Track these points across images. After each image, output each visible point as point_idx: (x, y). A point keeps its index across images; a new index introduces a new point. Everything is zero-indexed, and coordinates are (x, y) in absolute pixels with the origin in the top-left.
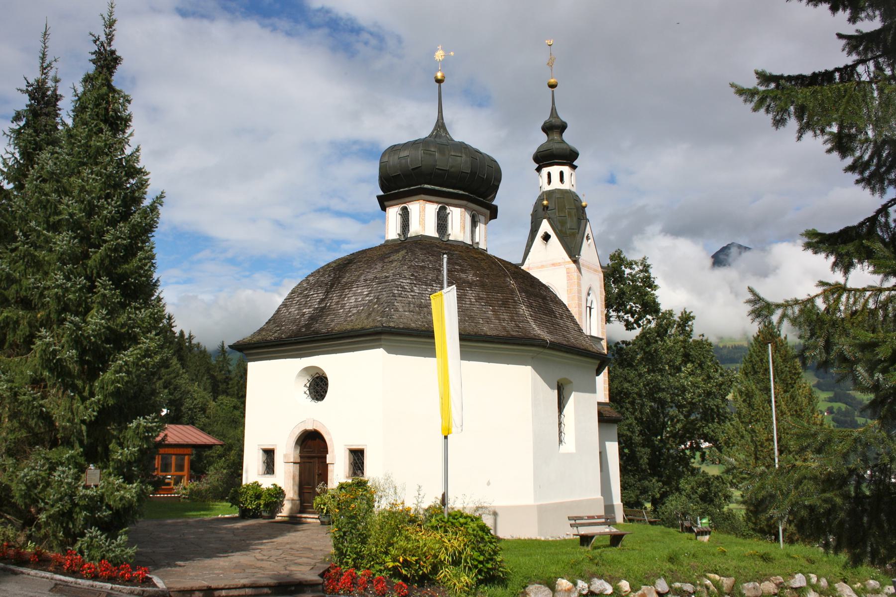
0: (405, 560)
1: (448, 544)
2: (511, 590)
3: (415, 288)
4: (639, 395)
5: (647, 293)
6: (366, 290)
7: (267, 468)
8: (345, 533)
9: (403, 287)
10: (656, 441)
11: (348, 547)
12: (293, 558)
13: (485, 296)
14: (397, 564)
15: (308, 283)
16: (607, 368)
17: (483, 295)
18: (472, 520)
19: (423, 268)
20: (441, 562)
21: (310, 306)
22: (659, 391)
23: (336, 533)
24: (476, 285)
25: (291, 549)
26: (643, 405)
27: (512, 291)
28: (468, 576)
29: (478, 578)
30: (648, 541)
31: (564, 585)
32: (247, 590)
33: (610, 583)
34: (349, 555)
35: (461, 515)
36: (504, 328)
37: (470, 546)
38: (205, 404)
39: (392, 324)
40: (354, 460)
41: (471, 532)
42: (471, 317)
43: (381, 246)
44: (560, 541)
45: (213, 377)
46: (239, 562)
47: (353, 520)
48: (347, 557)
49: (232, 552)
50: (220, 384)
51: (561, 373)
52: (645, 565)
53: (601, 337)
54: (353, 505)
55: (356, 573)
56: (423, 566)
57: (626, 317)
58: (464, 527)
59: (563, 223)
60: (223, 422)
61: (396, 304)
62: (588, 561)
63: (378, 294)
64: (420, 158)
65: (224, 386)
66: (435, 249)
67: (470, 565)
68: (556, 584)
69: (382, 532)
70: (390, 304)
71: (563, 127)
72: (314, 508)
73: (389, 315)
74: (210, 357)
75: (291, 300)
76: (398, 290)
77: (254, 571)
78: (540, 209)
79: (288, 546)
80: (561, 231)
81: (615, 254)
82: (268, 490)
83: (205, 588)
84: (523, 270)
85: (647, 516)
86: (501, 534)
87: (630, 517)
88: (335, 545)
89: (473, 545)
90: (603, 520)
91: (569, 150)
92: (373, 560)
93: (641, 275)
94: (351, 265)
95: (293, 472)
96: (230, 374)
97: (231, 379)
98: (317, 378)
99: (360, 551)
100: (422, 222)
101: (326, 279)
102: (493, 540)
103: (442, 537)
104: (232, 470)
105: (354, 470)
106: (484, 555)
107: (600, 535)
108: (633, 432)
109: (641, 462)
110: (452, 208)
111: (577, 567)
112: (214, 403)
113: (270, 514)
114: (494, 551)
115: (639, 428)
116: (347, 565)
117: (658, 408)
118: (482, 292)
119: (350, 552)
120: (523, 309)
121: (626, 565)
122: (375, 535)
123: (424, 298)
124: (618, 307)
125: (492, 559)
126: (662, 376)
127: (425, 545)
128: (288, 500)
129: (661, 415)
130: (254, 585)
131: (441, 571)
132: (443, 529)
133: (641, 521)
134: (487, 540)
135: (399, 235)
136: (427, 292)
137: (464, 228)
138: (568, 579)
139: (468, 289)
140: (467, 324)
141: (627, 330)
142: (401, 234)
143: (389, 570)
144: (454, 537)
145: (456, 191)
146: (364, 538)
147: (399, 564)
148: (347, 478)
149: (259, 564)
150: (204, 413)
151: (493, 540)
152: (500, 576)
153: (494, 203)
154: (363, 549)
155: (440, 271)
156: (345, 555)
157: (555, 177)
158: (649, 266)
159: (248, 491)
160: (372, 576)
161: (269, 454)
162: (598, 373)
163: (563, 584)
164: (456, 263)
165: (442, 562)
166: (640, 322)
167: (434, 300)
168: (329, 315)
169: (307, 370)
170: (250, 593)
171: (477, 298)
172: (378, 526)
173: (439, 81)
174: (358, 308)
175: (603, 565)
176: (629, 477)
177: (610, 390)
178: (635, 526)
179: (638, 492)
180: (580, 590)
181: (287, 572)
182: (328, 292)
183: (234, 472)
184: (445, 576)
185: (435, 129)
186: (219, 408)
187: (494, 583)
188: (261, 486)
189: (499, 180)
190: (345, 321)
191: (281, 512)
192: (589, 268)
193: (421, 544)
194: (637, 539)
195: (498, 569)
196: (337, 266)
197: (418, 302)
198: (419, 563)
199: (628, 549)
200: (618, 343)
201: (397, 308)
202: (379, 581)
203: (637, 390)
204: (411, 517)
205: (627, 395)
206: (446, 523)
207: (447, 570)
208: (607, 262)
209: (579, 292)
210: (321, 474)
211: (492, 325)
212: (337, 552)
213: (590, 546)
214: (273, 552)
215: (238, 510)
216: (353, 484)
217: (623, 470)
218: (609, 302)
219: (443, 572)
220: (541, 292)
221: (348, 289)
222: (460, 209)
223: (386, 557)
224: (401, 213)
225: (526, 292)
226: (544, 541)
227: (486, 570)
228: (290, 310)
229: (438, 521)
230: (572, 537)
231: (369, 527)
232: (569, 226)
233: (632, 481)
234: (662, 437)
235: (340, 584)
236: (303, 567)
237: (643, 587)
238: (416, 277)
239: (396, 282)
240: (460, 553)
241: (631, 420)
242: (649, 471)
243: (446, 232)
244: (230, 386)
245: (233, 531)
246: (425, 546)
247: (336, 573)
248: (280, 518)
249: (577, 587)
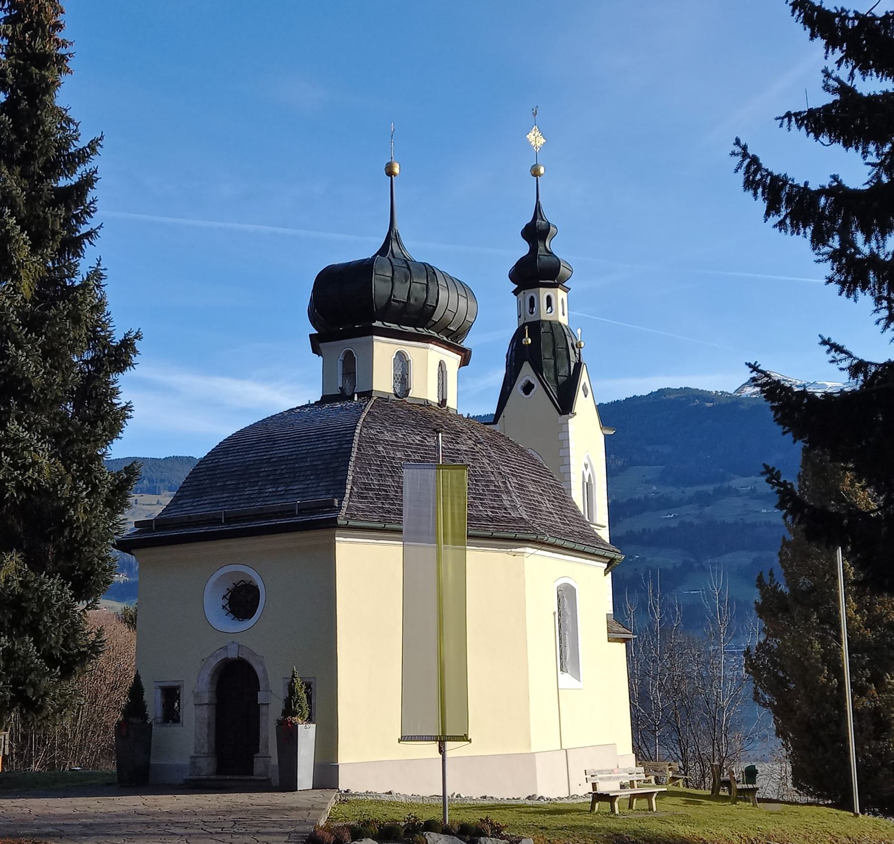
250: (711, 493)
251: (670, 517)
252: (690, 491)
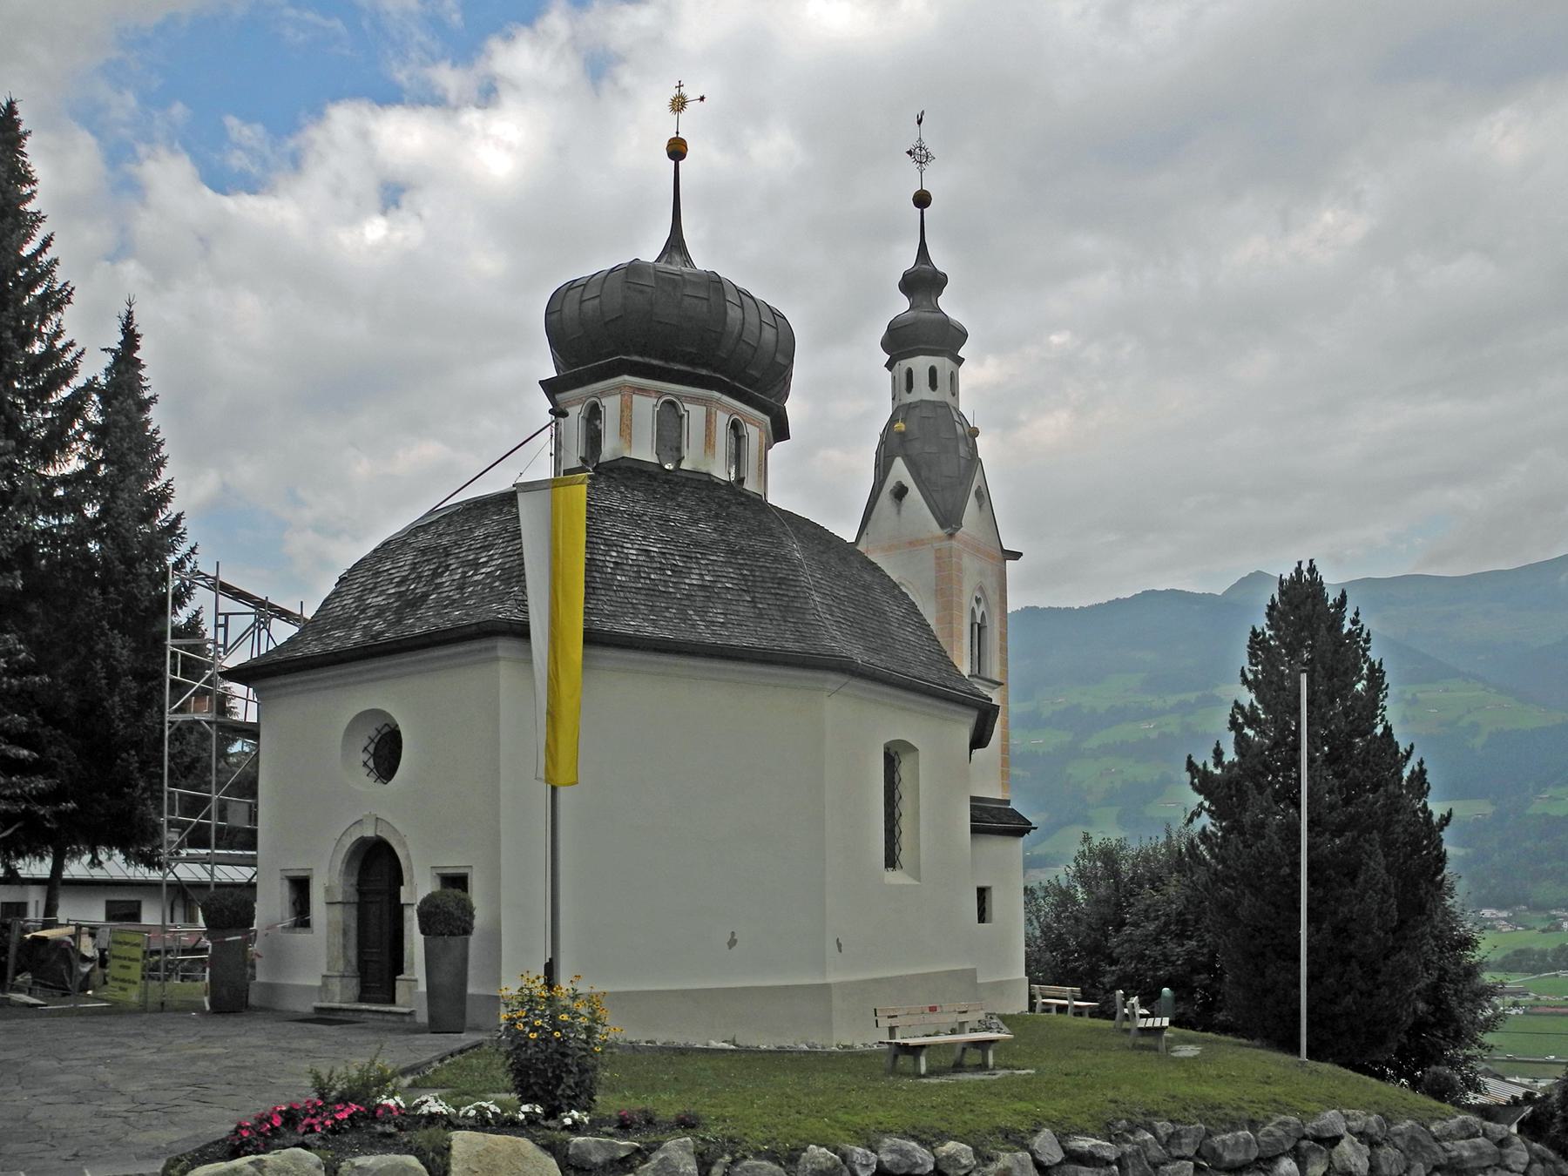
157: (921, 379)
161: (300, 886)
250: (1193, 701)
251: (1148, 728)
252: (1172, 700)
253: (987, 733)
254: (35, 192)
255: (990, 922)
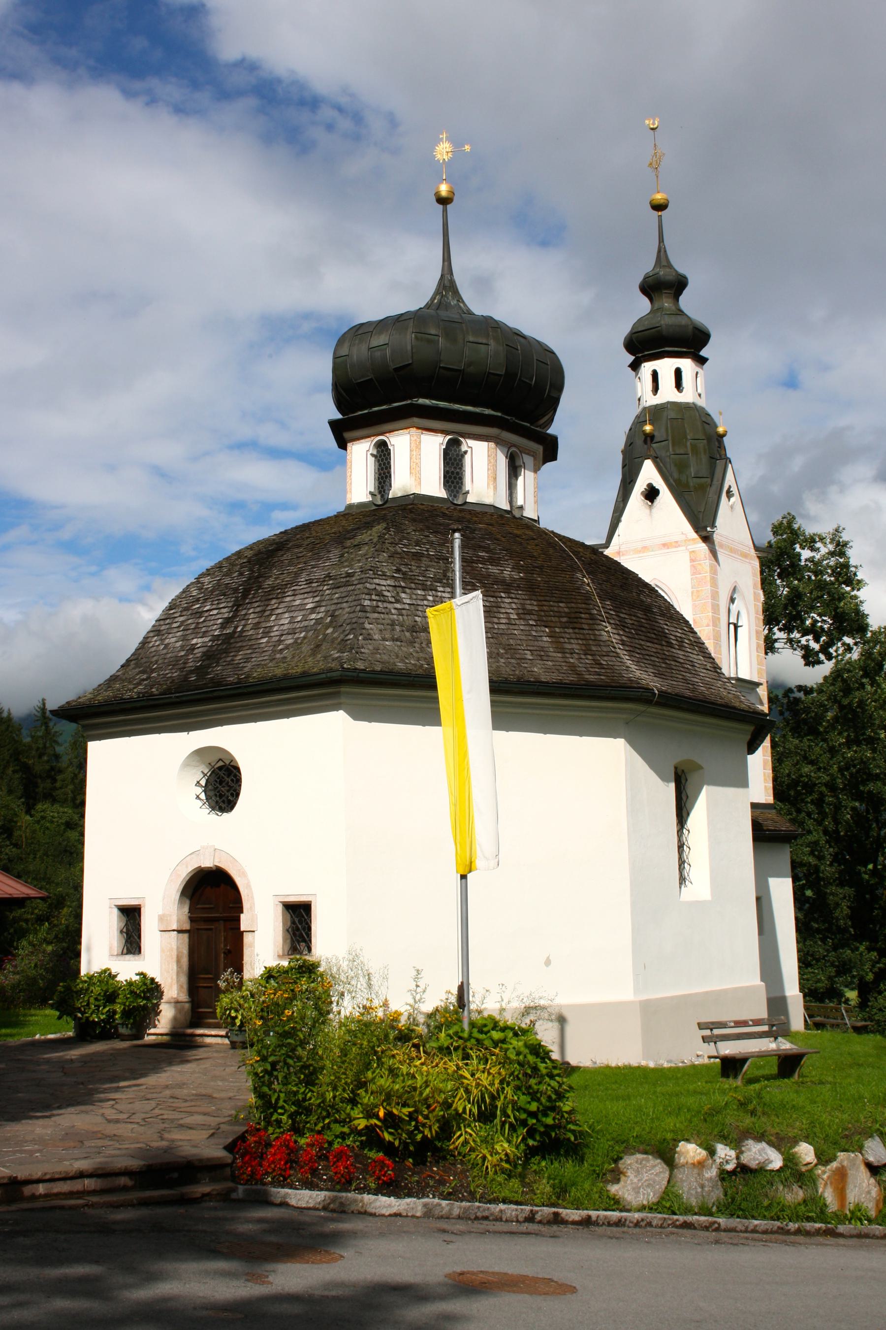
0: (389, 1114)
1: (470, 1081)
2: (592, 1165)
3: (403, 595)
4: (831, 787)
5: (842, 596)
6: (311, 600)
7: (126, 941)
8: (274, 1065)
9: (380, 594)
10: (865, 873)
11: (280, 1091)
12: (177, 1115)
13: (536, 608)
14: (374, 1121)
15: (200, 589)
16: (768, 738)
17: (532, 605)
18: (516, 1034)
19: (417, 556)
20: (458, 1116)
21: (205, 632)
22: (868, 780)
23: (256, 1065)
24: (519, 588)
25: (172, 1097)
26: (838, 807)
27: (587, 598)
28: (509, 1142)
29: (527, 1145)
30: (851, 1066)
31: (692, 1154)
32: (87, 1181)
33: (778, 1148)
34: (282, 1107)
35: (495, 1025)
36: (573, 667)
37: (512, 1084)
38: (11, 821)
39: (360, 665)
40: (293, 922)
41: (513, 1057)
42: (509, 648)
43: (339, 516)
44: (684, 1068)
45: (26, 769)
46: (73, 1126)
47: (289, 1041)
48: (280, 1111)
49: (59, 1108)
50: (39, 781)
51: (679, 752)
52: (843, 1112)
53: (756, 680)
54: (288, 1012)
55: (296, 1142)
56: (424, 1125)
57: (803, 641)
58: (501, 1048)
59: (682, 467)
60: (46, 854)
61: (367, 626)
62: (735, 1107)
63: (333, 607)
64: (409, 348)
65: (48, 784)
66: (441, 520)
67: (512, 1119)
68: (675, 1153)
69: (343, 1062)
70: (357, 627)
71: (679, 285)
72: (219, 1015)
73: (354, 648)
74: (19, 730)
75: (168, 621)
76: (370, 600)
77: (100, 1143)
78: (639, 441)
79: (168, 1092)
80: (678, 482)
81: (781, 523)
82: (130, 984)
83: (5, 1181)
84: (607, 557)
85: (848, 1016)
86: (573, 1059)
87: (818, 1019)
88: (255, 1088)
89: (517, 1083)
90: (765, 1028)
91: (691, 327)
92: (328, 1116)
93: (832, 562)
94: (281, 553)
95: (178, 948)
96: (58, 762)
97: (60, 771)
98: (220, 768)
99: (304, 1100)
100: (415, 469)
101: (234, 580)
102: (556, 1072)
103: (459, 1068)
104: (65, 945)
105: (292, 941)
106: (538, 1100)
107: (758, 1056)
108: (820, 858)
109: (837, 913)
110: (471, 442)
111: (715, 1118)
112: (28, 818)
113: (134, 1031)
114: (557, 1092)
115: (831, 850)
116: (280, 1127)
117: (867, 811)
118: (531, 600)
119: (285, 1101)
120: (608, 632)
121: (809, 1112)
122: (332, 1068)
123: (420, 613)
124: (789, 622)
125: (553, 1108)
126: (874, 750)
127: (427, 1084)
128: (168, 1002)
129: (874, 825)
130: (100, 1172)
131: (459, 1133)
132: (460, 1052)
133: (838, 1025)
134: (544, 1071)
135: (371, 493)
136: (426, 602)
137: (495, 479)
138: (699, 1142)
139: (503, 595)
140: (502, 660)
141: (806, 665)
142: (377, 493)
143: (359, 1133)
144: (481, 1067)
145: (478, 410)
146: (311, 1074)
147: (379, 1123)
148: (280, 957)
149: (111, 1129)
150: (10, 836)
151: (556, 1072)
152: (569, 1139)
153: (551, 431)
154: (309, 1095)
155: (447, 560)
156: (275, 1108)
158: (845, 544)
159: (92, 988)
160: (326, 1145)
162: (752, 748)
163: (688, 1152)
164: (480, 547)
165: (460, 1115)
166: (832, 650)
167: (434, 617)
168: (240, 648)
169: (201, 753)
170: (93, 1187)
171: (521, 611)
172: (337, 1051)
173: (443, 201)
174: (297, 636)
175: (764, 1114)
176: (816, 942)
177: (775, 780)
178: (825, 1036)
179: (832, 971)
180: (721, 1164)
181: (164, 1144)
182: (239, 606)
183: (68, 948)
184: (466, 1142)
185: (437, 292)
186: (37, 827)
187: (558, 1154)
188: (115, 976)
189: (559, 386)
190: (271, 660)
191: (155, 1026)
192: (732, 550)
193: (420, 1081)
194: (830, 1062)
195: (565, 1127)
196: (255, 555)
197: (408, 621)
198: (416, 1120)
199: (812, 1082)
200: (790, 690)
201: (369, 634)
202: (341, 1155)
203: (828, 778)
204: (400, 1031)
205: (810, 787)
206: (466, 1040)
207: (468, 1130)
208: (767, 537)
209: (715, 595)
210: (229, 951)
211: (550, 663)
212: (260, 1102)
213: (740, 1077)
214: (137, 1105)
215: (72, 1023)
216: (292, 969)
217: (803, 929)
218: (773, 613)
219: (461, 1135)
220: (642, 597)
221: (277, 598)
222: (486, 444)
223: (352, 1109)
224: (375, 452)
225: (613, 598)
226: (654, 1070)
227: (542, 1129)
228: (167, 641)
229: (451, 1038)
230: (706, 1061)
231: (320, 1053)
232: (692, 471)
233: (820, 949)
234: (875, 866)
235: (265, 1163)
236: (194, 1131)
237: (841, 1155)
238: (404, 574)
239: (368, 585)
240: (493, 1098)
241: (817, 835)
242: (852, 930)
243: (460, 488)
244: (58, 785)
245: (63, 1066)
246: (427, 1086)
247: (258, 1143)
248: (153, 1037)
249: (716, 1157)
253: (755, 745)
254: (824, 663)
255: (109, 960)
